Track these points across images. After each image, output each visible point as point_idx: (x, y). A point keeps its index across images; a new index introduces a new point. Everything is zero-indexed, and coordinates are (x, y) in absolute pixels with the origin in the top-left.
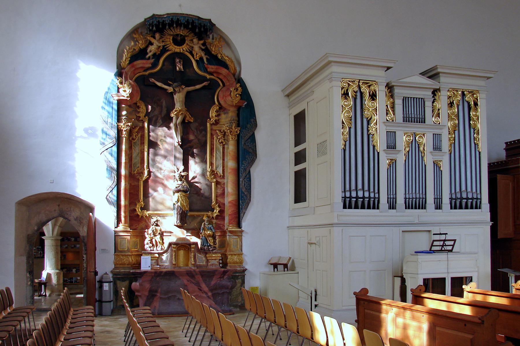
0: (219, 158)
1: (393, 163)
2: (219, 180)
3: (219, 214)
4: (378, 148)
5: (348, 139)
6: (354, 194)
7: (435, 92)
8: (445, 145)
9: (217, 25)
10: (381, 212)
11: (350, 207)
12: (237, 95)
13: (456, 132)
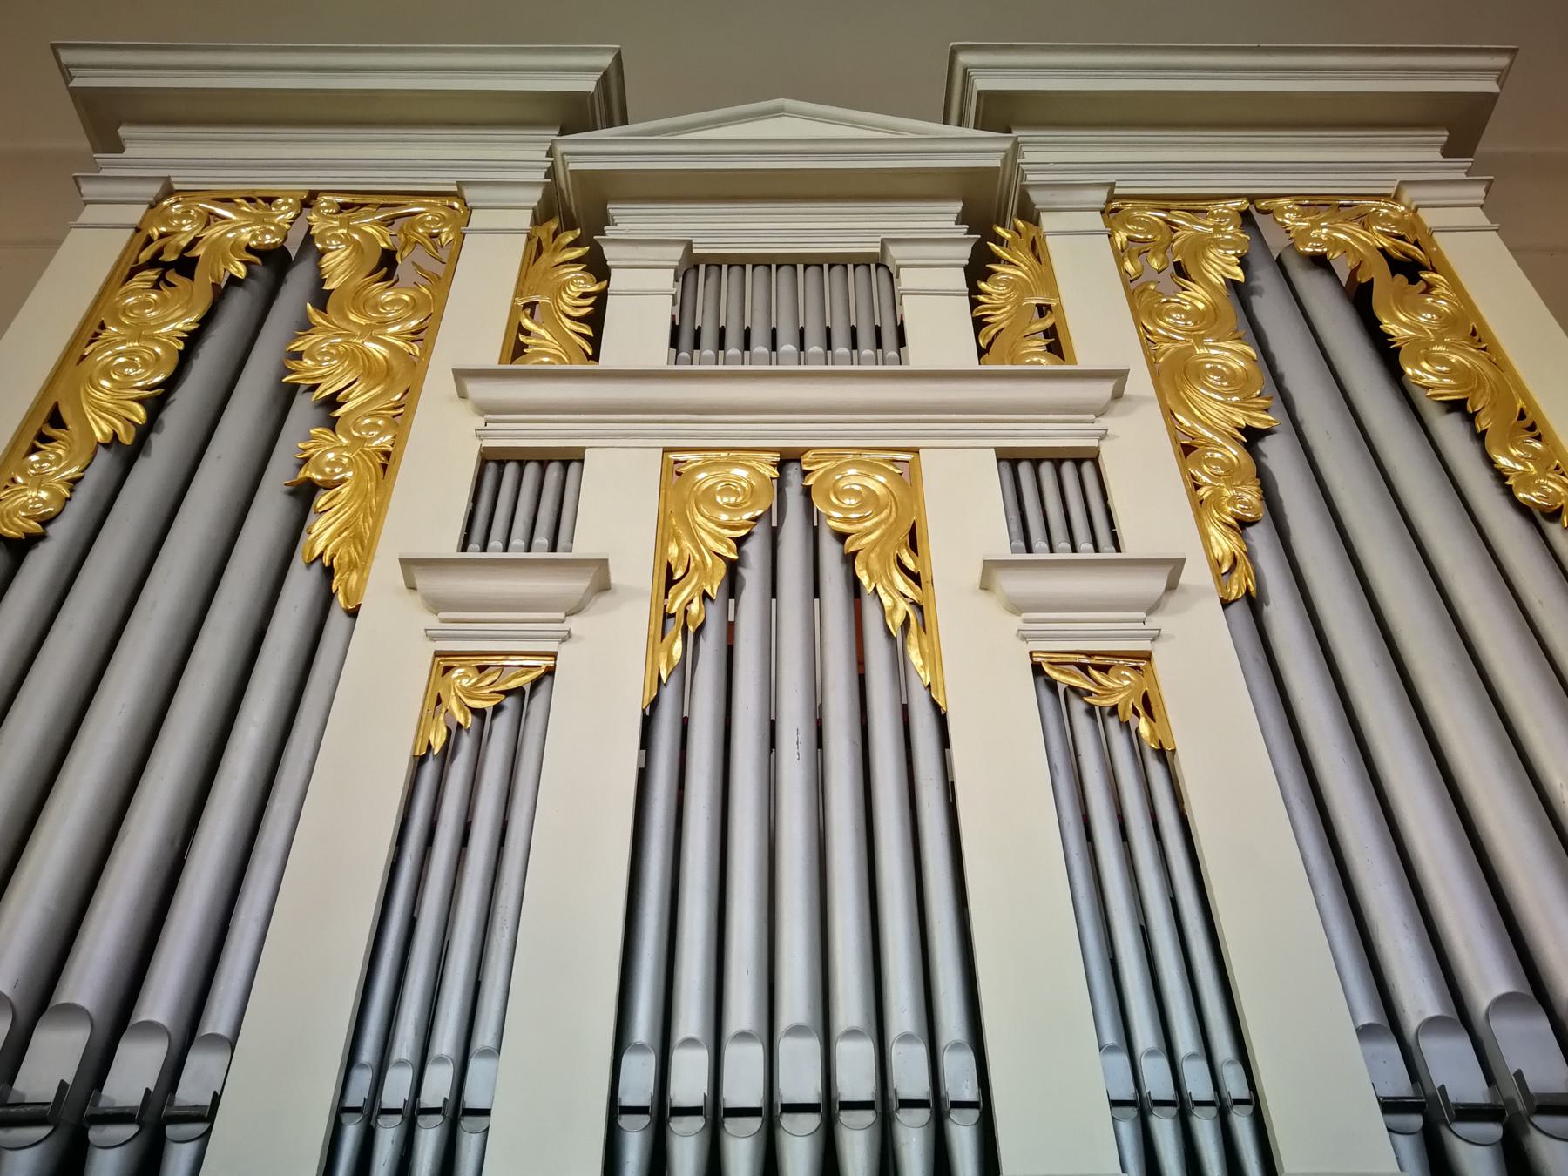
13: (1277, 452)
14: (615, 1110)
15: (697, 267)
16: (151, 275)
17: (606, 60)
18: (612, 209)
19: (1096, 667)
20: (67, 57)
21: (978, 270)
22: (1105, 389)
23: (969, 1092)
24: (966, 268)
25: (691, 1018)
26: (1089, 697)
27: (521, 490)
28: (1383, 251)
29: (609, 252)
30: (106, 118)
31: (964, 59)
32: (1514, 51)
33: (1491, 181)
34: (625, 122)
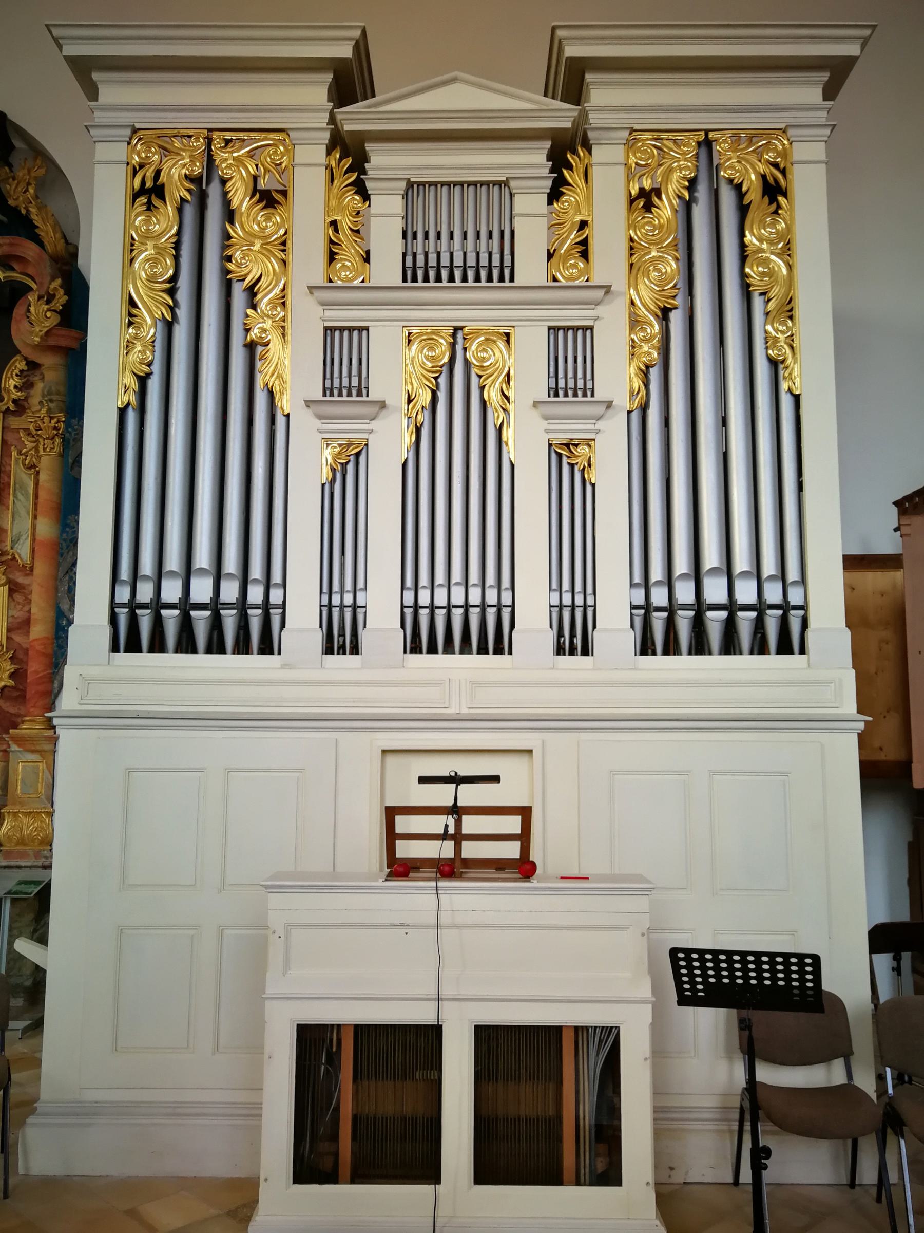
0: (23, 512)
1: (351, 461)
2: (21, 579)
3: (11, 683)
4: (285, 403)
5: (157, 368)
6: (172, 591)
7: (565, 151)
8: (616, 375)
9: (11, 116)
10: (284, 666)
11: (671, 647)
12: (49, 314)
13: (677, 320)
14: (403, 607)
15: (413, 186)
16: (143, 199)
17: (357, 33)
18: (368, 146)
19: (573, 445)
20: (56, 32)
21: (554, 195)
22: (601, 293)
23: (509, 603)
24: (549, 194)
25: (424, 580)
26: (567, 460)
27: (344, 350)
28: (764, 177)
29: (369, 185)
30: (84, 70)
31: (560, 33)
32: (874, 27)
33: (834, 126)
34: (374, 96)
